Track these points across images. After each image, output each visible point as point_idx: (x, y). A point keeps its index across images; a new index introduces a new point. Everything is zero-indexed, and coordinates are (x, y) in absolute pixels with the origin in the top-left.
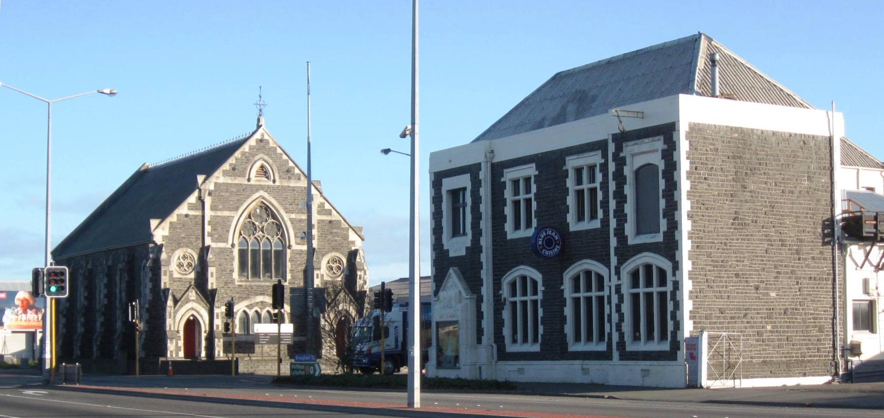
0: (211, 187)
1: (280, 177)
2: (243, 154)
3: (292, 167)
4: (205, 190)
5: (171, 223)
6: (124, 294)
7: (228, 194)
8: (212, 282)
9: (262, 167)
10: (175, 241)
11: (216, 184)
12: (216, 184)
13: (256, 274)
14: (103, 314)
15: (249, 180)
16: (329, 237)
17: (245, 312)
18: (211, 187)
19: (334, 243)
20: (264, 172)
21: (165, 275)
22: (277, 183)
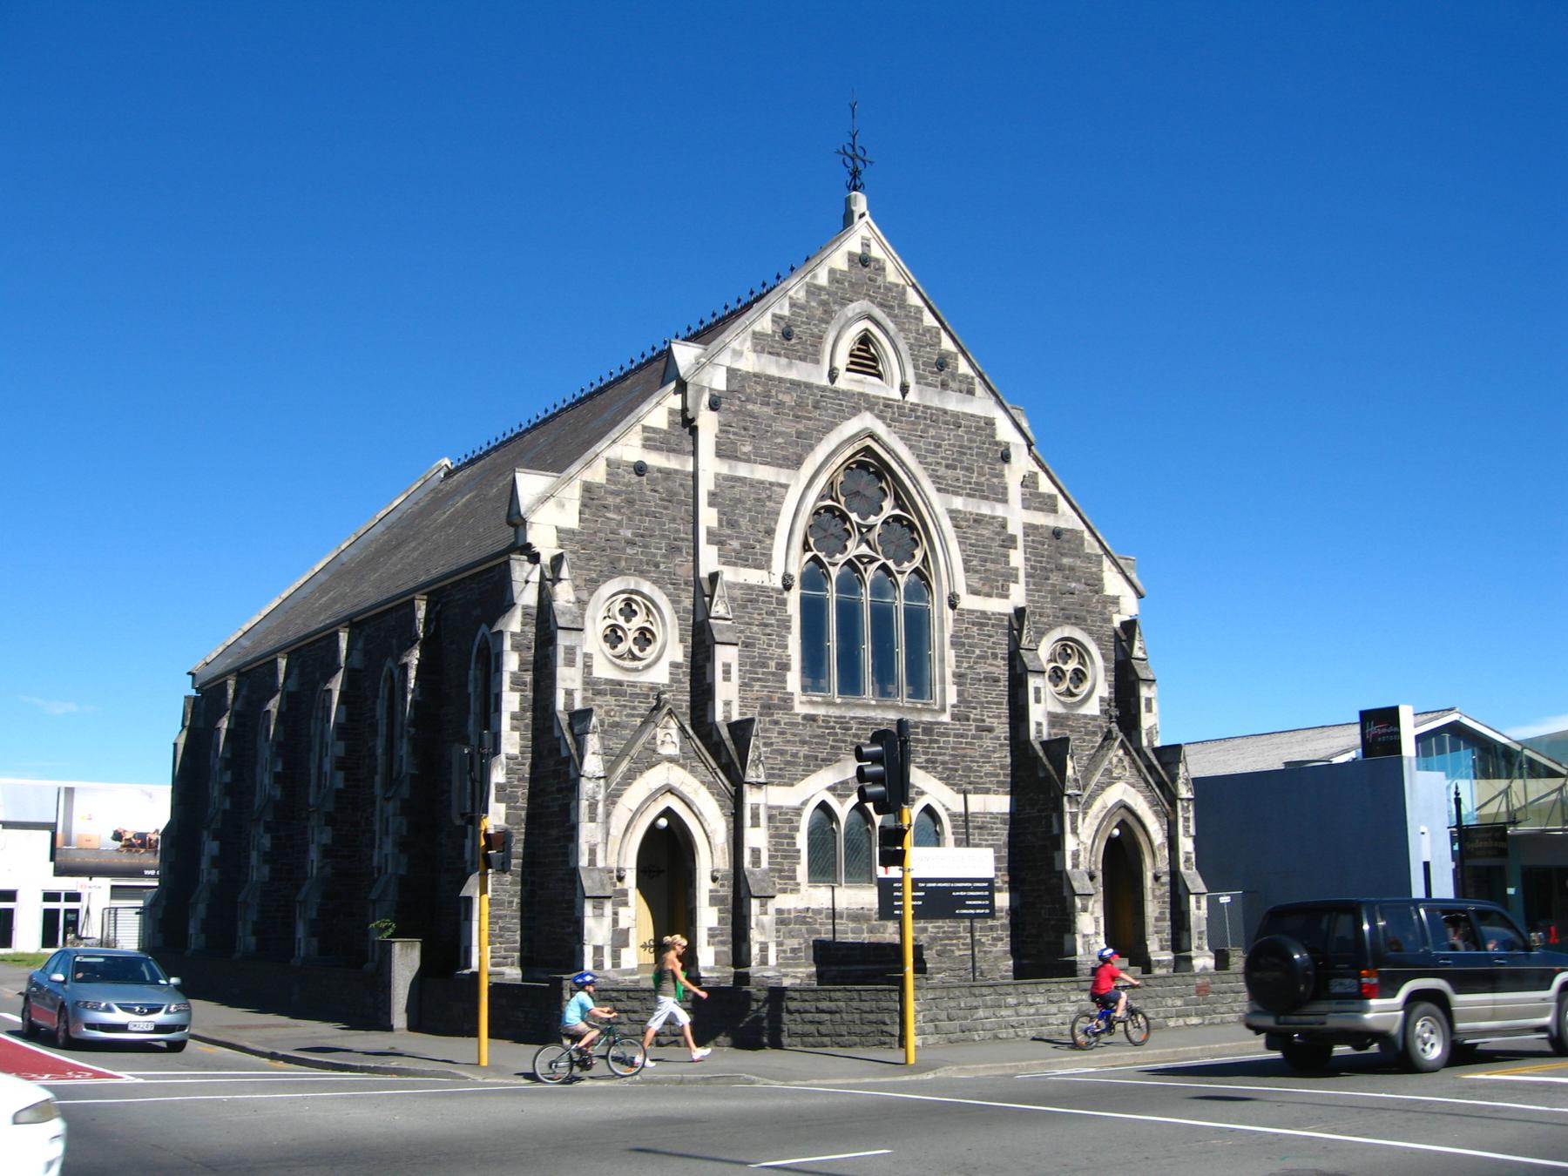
0: (719, 382)
1: (919, 379)
2: (813, 290)
3: (949, 354)
4: (701, 389)
5: (588, 488)
6: (404, 749)
7: (769, 411)
8: (728, 700)
9: (865, 340)
10: (595, 552)
11: (732, 373)
12: (732, 373)
13: (850, 685)
14: (330, 820)
15: (833, 376)
16: (1055, 578)
17: (823, 806)
18: (719, 382)
19: (1068, 598)
20: (866, 358)
21: (570, 662)
22: (912, 397)
